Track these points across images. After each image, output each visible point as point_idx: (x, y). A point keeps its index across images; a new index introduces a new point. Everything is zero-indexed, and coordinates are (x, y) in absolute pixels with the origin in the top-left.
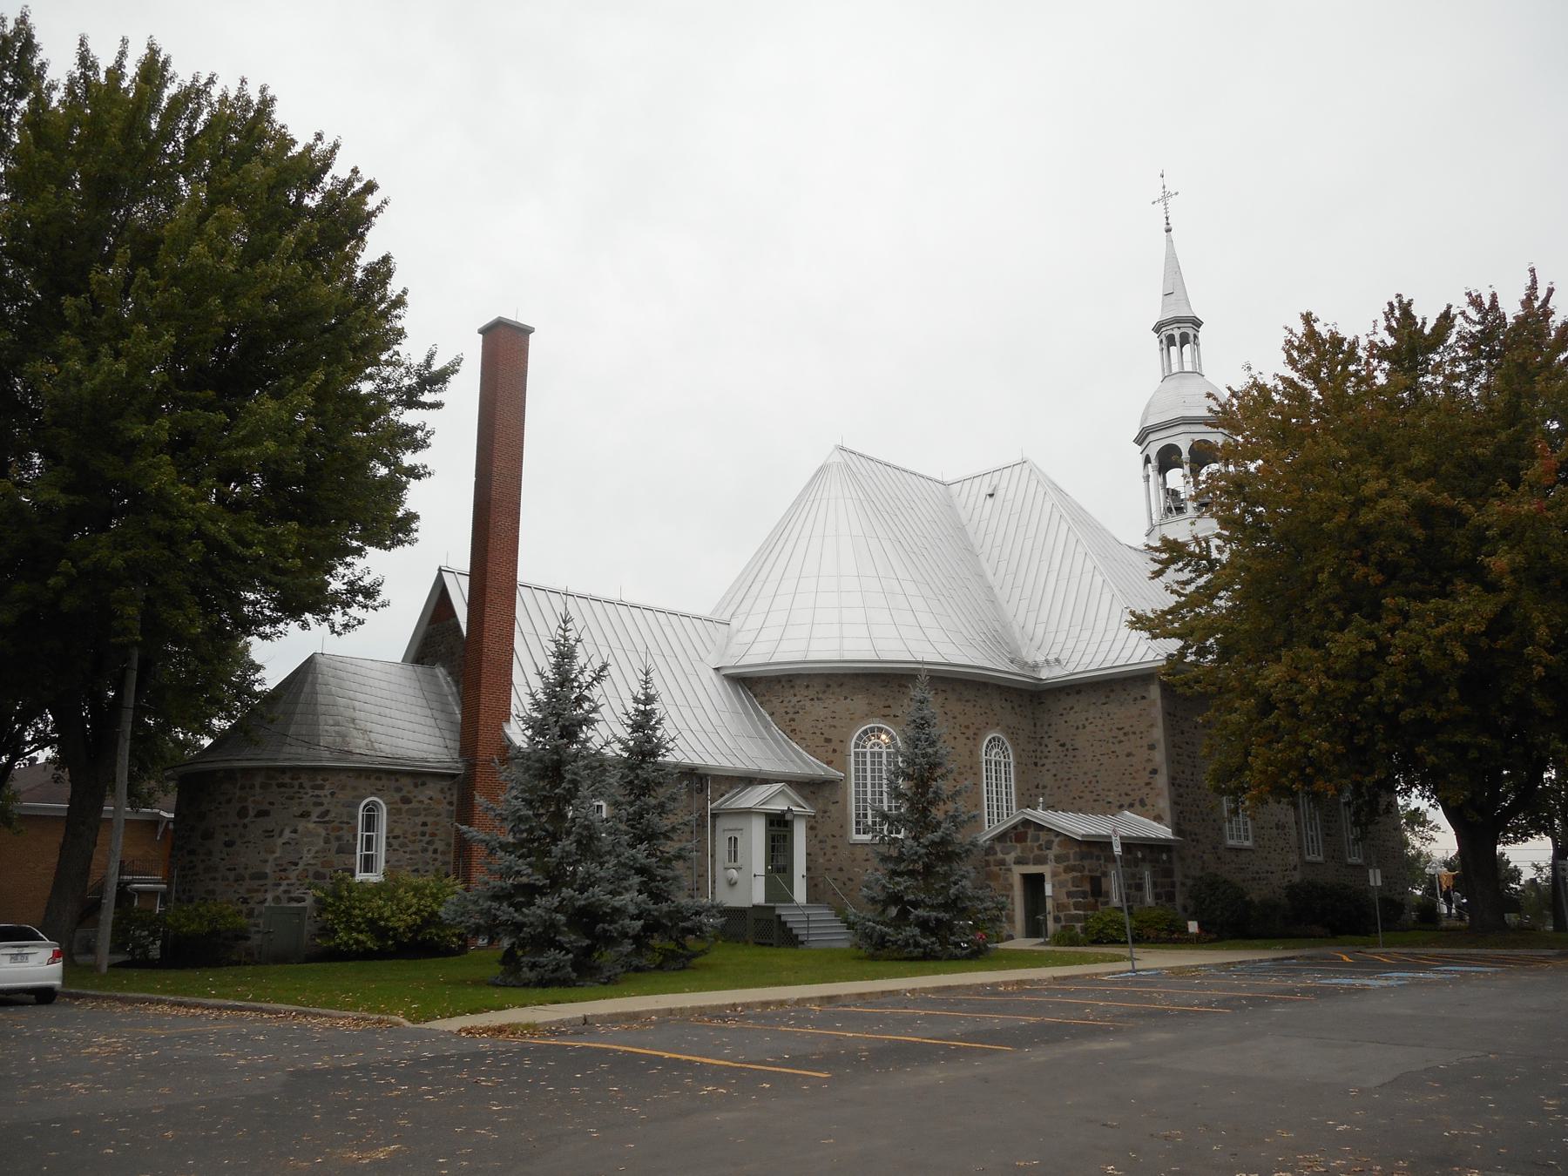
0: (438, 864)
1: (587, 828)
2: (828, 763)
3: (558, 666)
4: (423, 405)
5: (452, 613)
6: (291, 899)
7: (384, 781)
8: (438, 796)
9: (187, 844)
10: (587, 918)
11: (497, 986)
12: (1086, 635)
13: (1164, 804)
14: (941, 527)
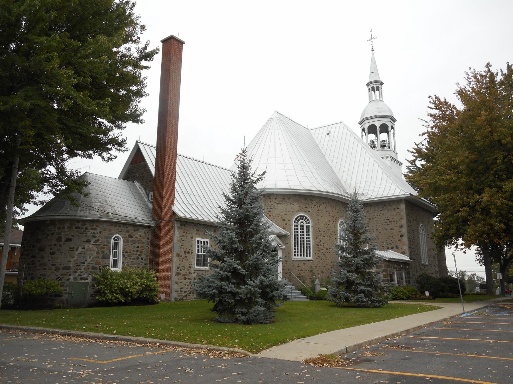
2: (284, 229)
6: (82, 279)
7: (122, 228)
11: (221, 322)
13: (406, 248)
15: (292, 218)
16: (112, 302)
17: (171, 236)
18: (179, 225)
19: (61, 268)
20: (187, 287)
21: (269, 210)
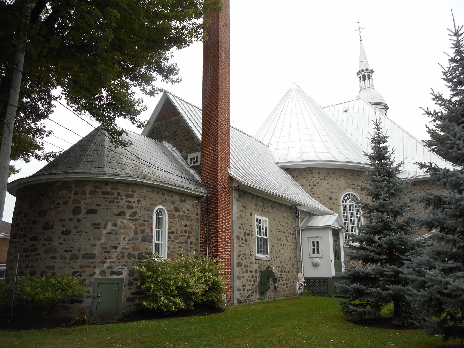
6: (113, 273)
7: (165, 197)
8: (191, 209)
16: (169, 311)
17: (229, 210)
18: (237, 197)
19: (80, 256)
20: (249, 283)
21: (312, 186)
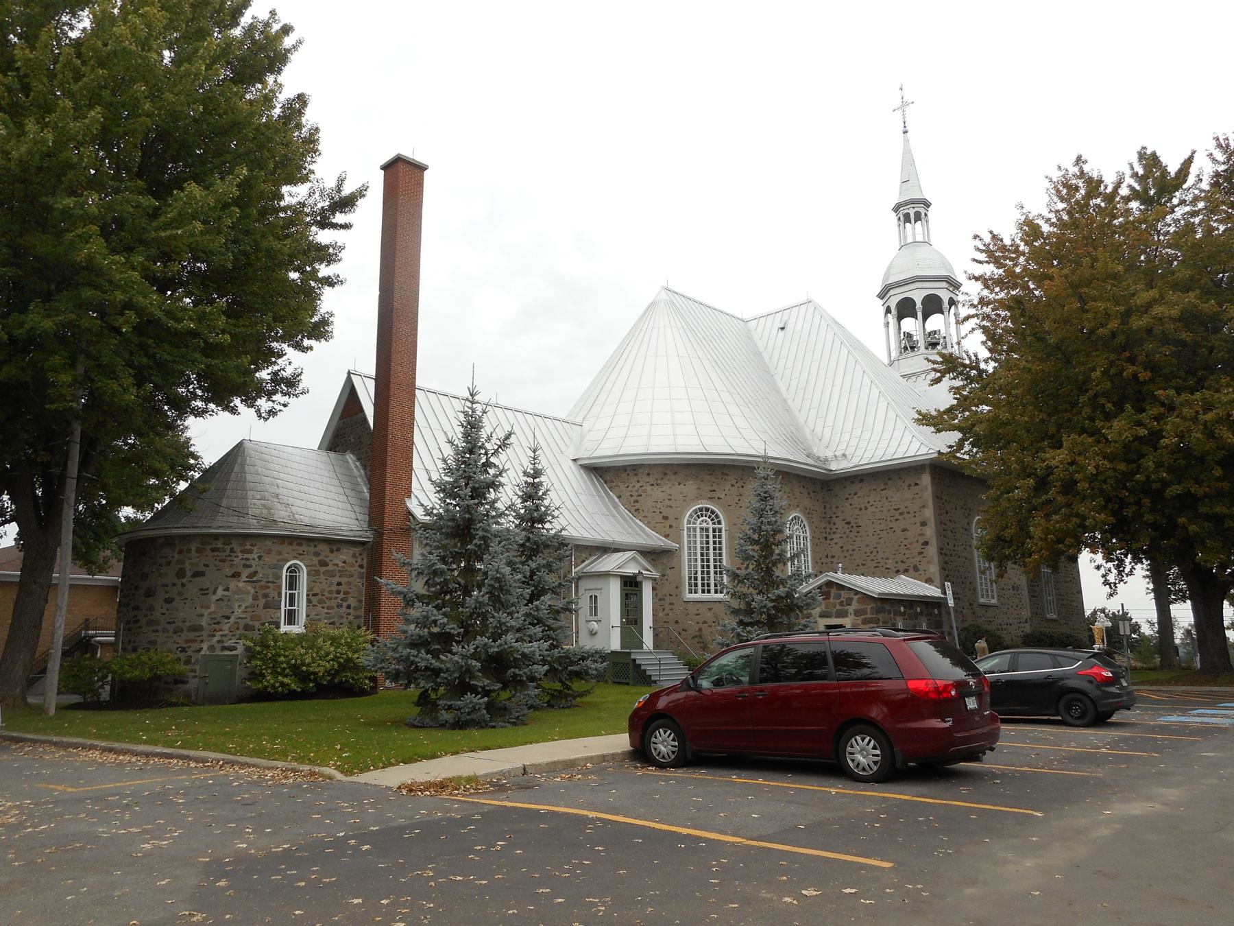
0: (351, 618)
1: (497, 580)
2: (666, 536)
3: (466, 435)
4: (335, 226)
5: (361, 410)
6: (224, 648)
7: (305, 547)
9: (132, 600)
10: (498, 664)
11: (417, 727)
12: (866, 435)
13: (934, 569)
14: (742, 353)
15: (683, 513)
21: (635, 498)
